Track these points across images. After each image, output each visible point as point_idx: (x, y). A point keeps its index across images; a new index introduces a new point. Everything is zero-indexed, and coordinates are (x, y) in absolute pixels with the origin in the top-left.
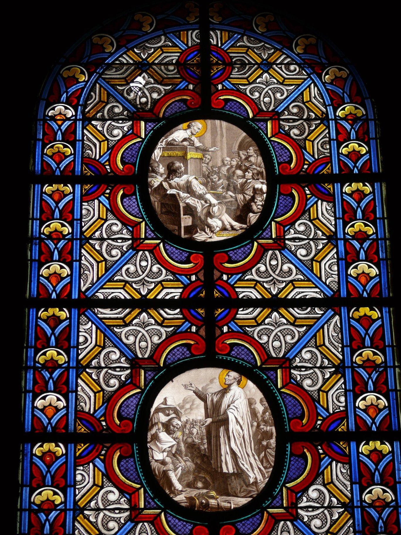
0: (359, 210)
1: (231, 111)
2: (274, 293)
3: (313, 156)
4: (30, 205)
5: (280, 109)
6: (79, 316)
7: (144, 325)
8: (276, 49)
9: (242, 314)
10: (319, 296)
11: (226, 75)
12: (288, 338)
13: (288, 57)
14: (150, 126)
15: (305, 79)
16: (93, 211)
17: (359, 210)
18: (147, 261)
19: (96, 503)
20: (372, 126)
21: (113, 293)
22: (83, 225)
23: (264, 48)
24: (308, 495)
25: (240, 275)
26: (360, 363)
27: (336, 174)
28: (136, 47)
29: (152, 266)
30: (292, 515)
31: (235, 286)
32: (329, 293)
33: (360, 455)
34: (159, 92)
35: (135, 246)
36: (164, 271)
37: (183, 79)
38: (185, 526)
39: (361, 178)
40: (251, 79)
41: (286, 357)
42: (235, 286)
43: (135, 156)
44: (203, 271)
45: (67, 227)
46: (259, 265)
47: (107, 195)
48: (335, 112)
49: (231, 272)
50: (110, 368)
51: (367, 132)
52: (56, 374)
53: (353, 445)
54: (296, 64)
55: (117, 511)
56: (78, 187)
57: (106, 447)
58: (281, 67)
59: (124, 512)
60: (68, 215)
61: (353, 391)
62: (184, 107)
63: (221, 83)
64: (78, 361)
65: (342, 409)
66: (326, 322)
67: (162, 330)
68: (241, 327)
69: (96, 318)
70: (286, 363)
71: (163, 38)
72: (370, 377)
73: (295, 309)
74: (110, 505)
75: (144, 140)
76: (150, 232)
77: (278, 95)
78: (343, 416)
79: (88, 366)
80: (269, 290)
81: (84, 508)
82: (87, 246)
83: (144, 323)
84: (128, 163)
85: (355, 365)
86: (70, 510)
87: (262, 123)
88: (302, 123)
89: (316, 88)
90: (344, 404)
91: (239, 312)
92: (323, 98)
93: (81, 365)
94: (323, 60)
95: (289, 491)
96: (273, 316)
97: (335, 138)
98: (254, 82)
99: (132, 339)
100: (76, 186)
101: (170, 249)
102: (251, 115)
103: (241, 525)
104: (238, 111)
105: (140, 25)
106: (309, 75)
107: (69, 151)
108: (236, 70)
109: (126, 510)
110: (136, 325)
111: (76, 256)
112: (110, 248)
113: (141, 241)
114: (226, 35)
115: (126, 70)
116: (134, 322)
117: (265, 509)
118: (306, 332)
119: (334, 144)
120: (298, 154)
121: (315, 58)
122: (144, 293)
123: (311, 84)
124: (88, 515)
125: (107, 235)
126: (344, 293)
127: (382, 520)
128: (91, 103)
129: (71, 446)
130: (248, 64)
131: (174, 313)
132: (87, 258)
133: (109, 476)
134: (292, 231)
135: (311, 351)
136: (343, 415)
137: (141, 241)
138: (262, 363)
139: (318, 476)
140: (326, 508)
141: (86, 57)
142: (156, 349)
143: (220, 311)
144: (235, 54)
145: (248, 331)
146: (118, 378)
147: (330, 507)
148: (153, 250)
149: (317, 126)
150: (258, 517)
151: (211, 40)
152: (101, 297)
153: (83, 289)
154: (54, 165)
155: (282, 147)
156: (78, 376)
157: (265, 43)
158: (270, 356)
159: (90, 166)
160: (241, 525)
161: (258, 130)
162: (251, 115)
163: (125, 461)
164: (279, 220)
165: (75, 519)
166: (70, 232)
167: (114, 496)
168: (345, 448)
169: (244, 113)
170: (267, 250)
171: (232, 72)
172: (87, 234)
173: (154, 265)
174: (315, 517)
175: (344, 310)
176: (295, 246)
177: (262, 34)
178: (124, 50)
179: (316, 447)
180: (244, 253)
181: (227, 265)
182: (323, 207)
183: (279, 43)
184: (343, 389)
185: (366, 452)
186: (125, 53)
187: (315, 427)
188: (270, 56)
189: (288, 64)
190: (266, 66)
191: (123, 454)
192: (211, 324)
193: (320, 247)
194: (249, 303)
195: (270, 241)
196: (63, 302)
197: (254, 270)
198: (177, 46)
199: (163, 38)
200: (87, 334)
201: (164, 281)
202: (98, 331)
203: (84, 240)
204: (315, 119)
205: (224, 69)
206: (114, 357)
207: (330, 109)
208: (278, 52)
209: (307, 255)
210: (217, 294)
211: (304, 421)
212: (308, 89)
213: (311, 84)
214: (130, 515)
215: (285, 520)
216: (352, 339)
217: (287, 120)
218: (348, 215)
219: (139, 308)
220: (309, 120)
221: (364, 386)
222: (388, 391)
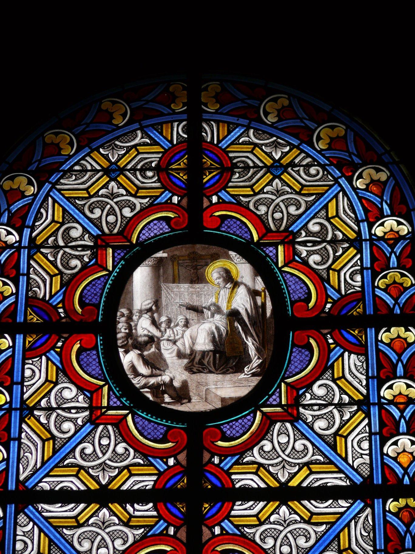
0: (400, 365)
1: (229, 233)
5: (294, 228)
6: (17, 514)
7: (105, 525)
8: (292, 147)
10: (344, 484)
11: (223, 183)
13: (308, 156)
14: (119, 254)
15: (331, 186)
17: (400, 365)
18: (109, 438)
19: (54, 240)
21: (62, 482)
22: (25, 391)
23: (276, 145)
24: (312, 392)
25: (237, 457)
26: (389, 397)
27: (370, 315)
28: (102, 146)
29: (116, 445)
30: (291, 415)
31: (228, 149)
33: (379, 343)
34: (132, 207)
35: (94, 417)
37: (164, 187)
38: (156, 429)
40: (257, 188)
41: (290, 229)
42: (228, 149)
43: (99, 294)
44: (185, 452)
45: (13, 235)
47: (58, 350)
48: (370, 229)
49: (224, 453)
53: (371, 332)
54: (319, 165)
55: (73, 411)
56: (19, 338)
57: (63, 338)
58: (299, 171)
59: (82, 412)
62: (166, 229)
63: (219, 524)
69: (40, 517)
70: (289, 239)
71: (139, 133)
73: (312, 502)
74: (71, 242)
75: (111, 273)
76: (271, 254)
77: (301, 541)
78: (359, 297)
79: (37, 407)
80: (270, 155)
83: (103, 523)
84: (89, 304)
85: (383, 400)
86: (16, 409)
87: (271, 249)
88: (325, 247)
89: (346, 199)
90: (359, 284)
92: (354, 212)
93: (27, 405)
94: (354, 157)
95: (289, 388)
96: (274, 184)
97: (369, 266)
98: (261, 191)
100: (17, 336)
101: (141, 423)
102: (256, 237)
103: (228, 427)
104: (238, 232)
106: (336, 180)
108: (237, 175)
110: (95, 524)
112: (67, 258)
113: (103, 410)
114: (224, 130)
115: (90, 178)
116: (91, 521)
119: (368, 274)
120: (319, 297)
121: (344, 156)
123: (339, 192)
124: (38, 416)
125: (57, 403)
126: (378, 480)
127: (402, 363)
128: (41, 225)
130: (253, 167)
132: (29, 435)
133: (66, 371)
134: (304, 234)
135: (326, 384)
136: (359, 296)
137: (103, 410)
140: (329, 242)
141: (35, 162)
142: (128, 223)
144: (238, 154)
145: (242, 201)
146: (74, 421)
148: (119, 424)
149: (345, 250)
150: (249, 417)
151: (203, 134)
155: (297, 280)
156: (22, 420)
157: (278, 137)
158: (269, 230)
159: (35, 309)
160: (228, 427)
161: (265, 257)
162: (256, 237)
163: (85, 355)
164: (289, 380)
166: (14, 292)
168: (361, 337)
169: (246, 235)
171: (231, 178)
173: (119, 443)
174: (320, 417)
175: (378, 503)
176: (312, 416)
177: (272, 125)
178: (87, 150)
179: (325, 336)
180: (150, 229)
181: (220, 443)
182: (353, 361)
184: (359, 266)
186: (88, 155)
187: (323, 311)
189: (309, 166)
190: (277, 169)
191: (84, 346)
192: (195, 468)
193: (347, 417)
194: (249, 494)
198: (157, 144)
199: (139, 133)
201: (139, 145)
202: (42, 534)
204: (343, 241)
207: (364, 226)
208: (295, 149)
212: (334, 200)
213: (339, 192)
215: (283, 421)
217: (304, 244)
219: (97, 502)
220: (334, 242)
221: (393, 427)
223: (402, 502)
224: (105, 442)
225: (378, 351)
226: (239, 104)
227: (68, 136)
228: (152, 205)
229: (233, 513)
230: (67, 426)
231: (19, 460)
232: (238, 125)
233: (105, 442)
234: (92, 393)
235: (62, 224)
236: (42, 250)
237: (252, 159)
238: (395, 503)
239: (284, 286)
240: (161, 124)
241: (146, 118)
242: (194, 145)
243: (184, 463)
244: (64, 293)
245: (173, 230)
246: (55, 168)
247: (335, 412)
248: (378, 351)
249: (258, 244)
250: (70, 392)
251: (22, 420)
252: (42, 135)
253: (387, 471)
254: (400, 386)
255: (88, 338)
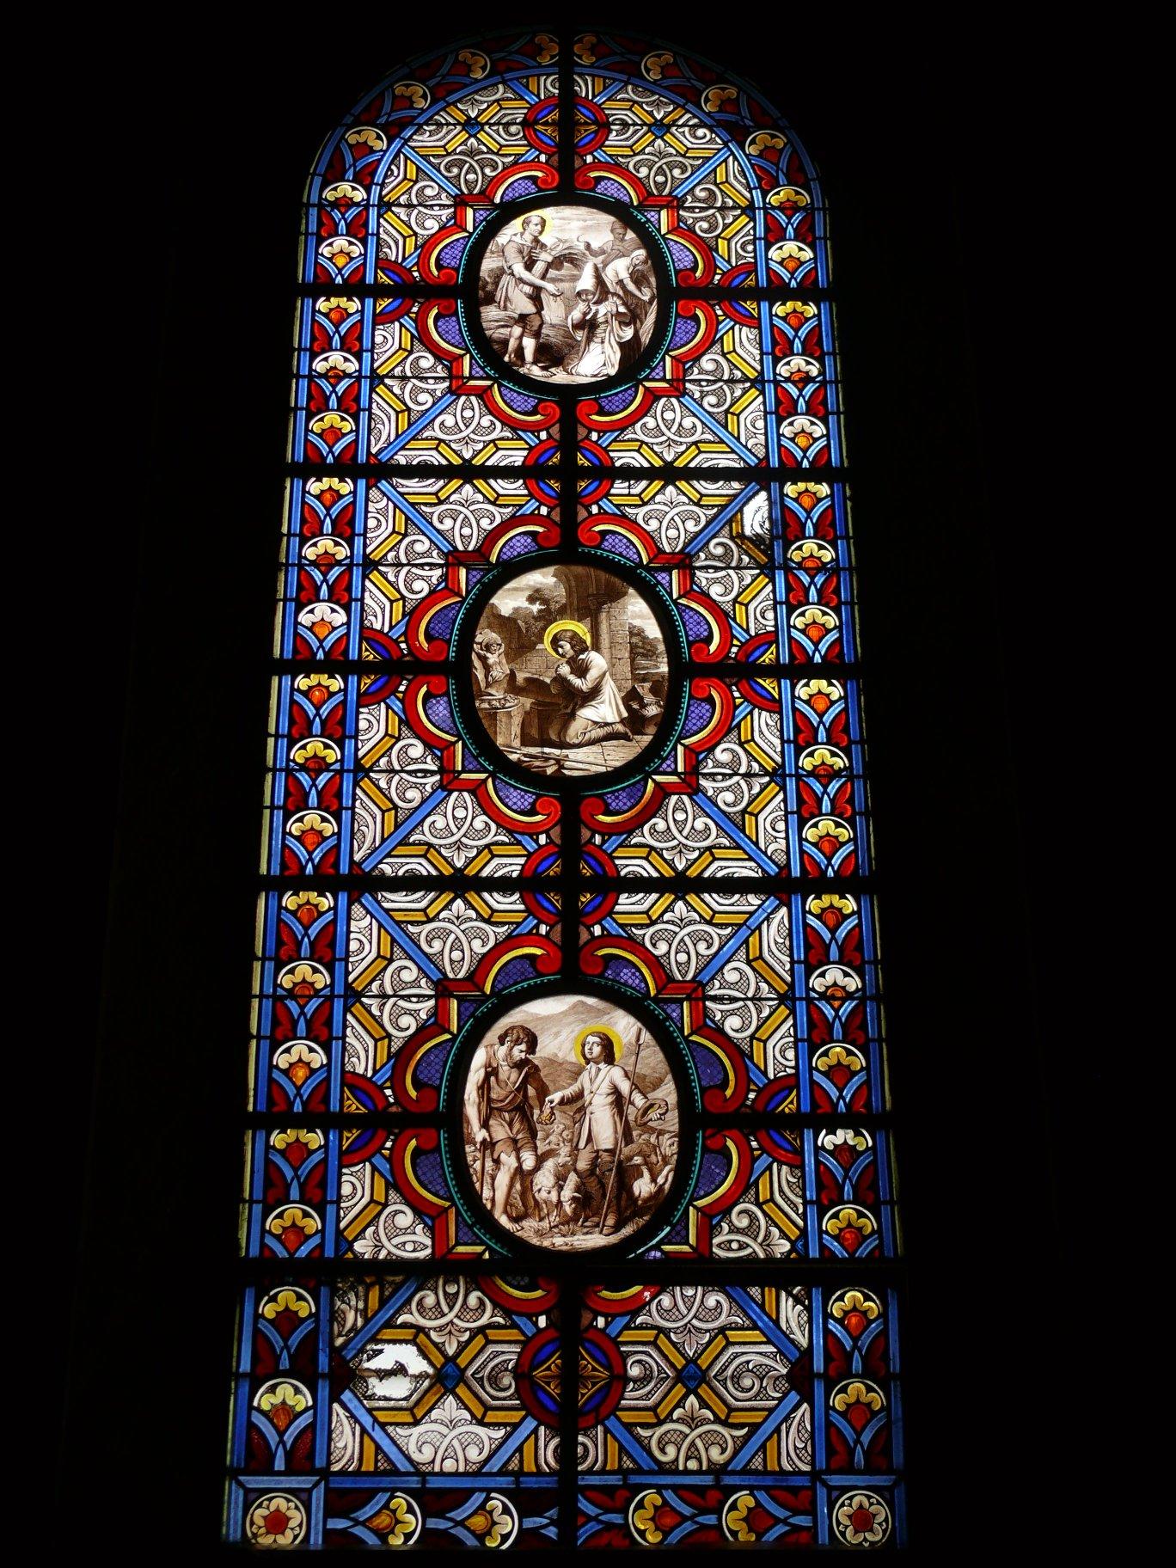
2: (680, 903)
3: (729, 262)
4: (293, 324)
8: (677, 106)
9: (625, 902)
12: (702, 946)
13: (695, 116)
16: (390, 340)
20: (819, 218)
28: (459, 101)
32: (753, 461)
36: (498, 424)
39: (839, 886)
40: (637, 148)
46: (654, 821)
50: (402, 997)
51: (812, 229)
52: (322, 779)
60: (354, 344)
61: (776, 412)
62: (533, 188)
64: (357, 760)
65: (790, 1071)
66: (786, 1419)
67: (482, 1431)
68: (617, 506)
70: (696, 991)
71: (501, 87)
72: (812, 582)
75: (471, 234)
78: (770, 639)
79: (390, 375)
81: (371, 769)
82: (375, 576)
90: (793, 1064)
91: (627, 1395)
99: (448, 523)
105: (469, 69)
106: (725, 144)
107: (347, 426)
109: (433, 773)
111: (356, 593)
112: (415, 391)
114: (600, 83)
117: (640, 382)
118: (747, 1438)
122: (459, 864)
126: (774, 462)
128: (392, 182)
129: (353, 679)
131: (508, 903)
134: (710, 763)
136: (793, 1081)
138: (659, 992)
139: (713, 343)
140: (726, 382)
142: (480, 961)
143: (583, 484)
147: (748, 775)
148: (477, 790)
152: (403, 461)
153: (374, 451)
154: (324, 449)
156: (365, 577)
158: (671, 979)
165: (356, 784)
167: (417, 750)
170: (659, 398)
172: (376, 556)
175: (774, 486)
178: (442, 104)
181: (602, 818)
182: (764, 719)
183: (682, 96)
185: (816, 911)
186: (443, 109)
188: (667, 114)
195: (674, 779)
196: (325, 881)
197: (646, 828)
200: (363, 935)
203: (353, 996)
204: (733, 208)
205: (596, 132)
206: (407, 976)
207: (757, 194)
209: (718, 405)
210: (585, 898)
211: (729, 1093)
214: (449, 387)
216: (774, 343)
217: (691, 209)
218: (780, 348)
222: (868, 1040)
223: (801, 486)
224: (468, 413)
225: (795, 710)
226: (618, 59)
227: (419, 89)
228: (515, 163)
229: (617, 908)
230: (423, 397)
231: (353, 834)
232: (615, 80)
233: (456, 955)
234: (433, 1219)
235: (416, 182)
236: (387, 381)
237: (629, 117)
238: (830, 1137)
239: (693, 1182)
240: (527, 77)
241: (509, 69)
242: (568, 100)
243: (557, 437)
244: (393, 1067)
245: (541, 548)
246: (403, 124)
247: (742, 783)
248: (795, 710)
249: (656, 1000)
250: (427, 361)
251: (365, 577)
252: (391, 86)
253: (834, 1438)
254: (859, 1390)
255: (437, 680)
